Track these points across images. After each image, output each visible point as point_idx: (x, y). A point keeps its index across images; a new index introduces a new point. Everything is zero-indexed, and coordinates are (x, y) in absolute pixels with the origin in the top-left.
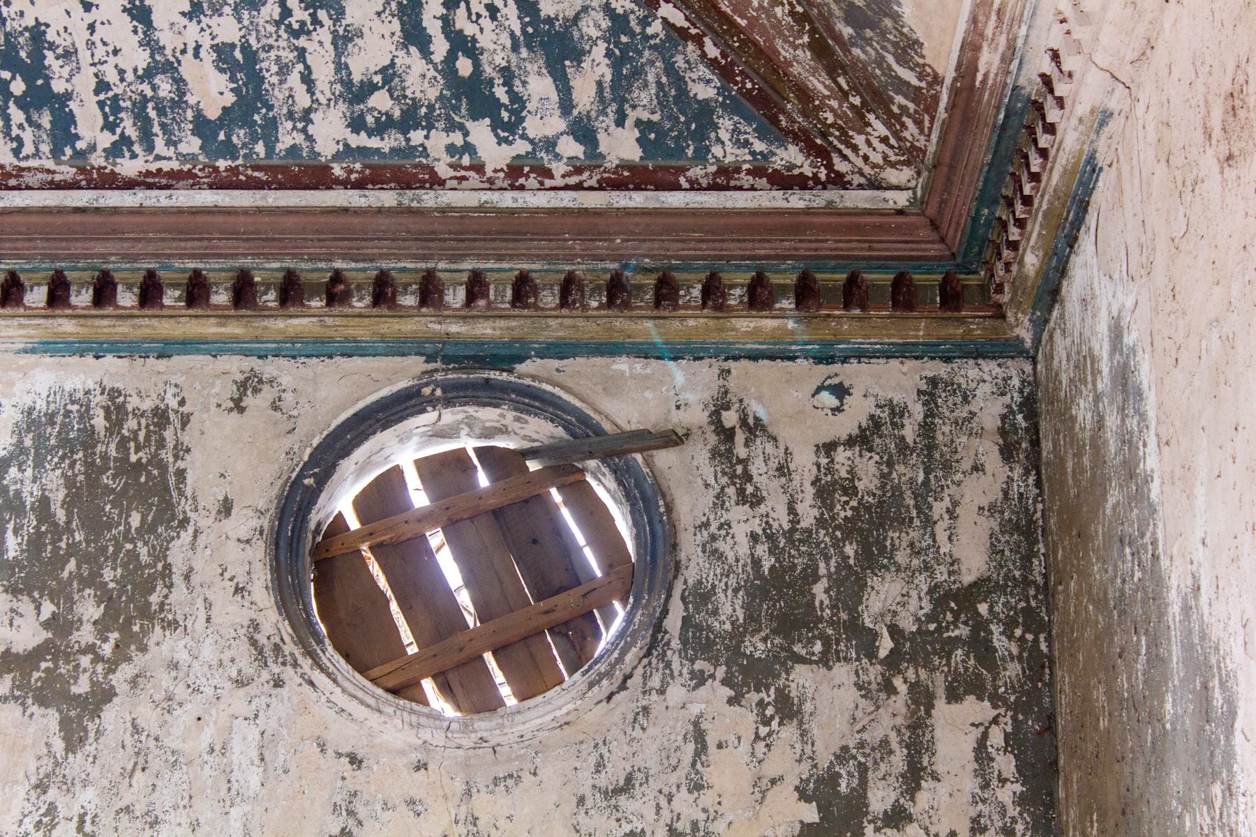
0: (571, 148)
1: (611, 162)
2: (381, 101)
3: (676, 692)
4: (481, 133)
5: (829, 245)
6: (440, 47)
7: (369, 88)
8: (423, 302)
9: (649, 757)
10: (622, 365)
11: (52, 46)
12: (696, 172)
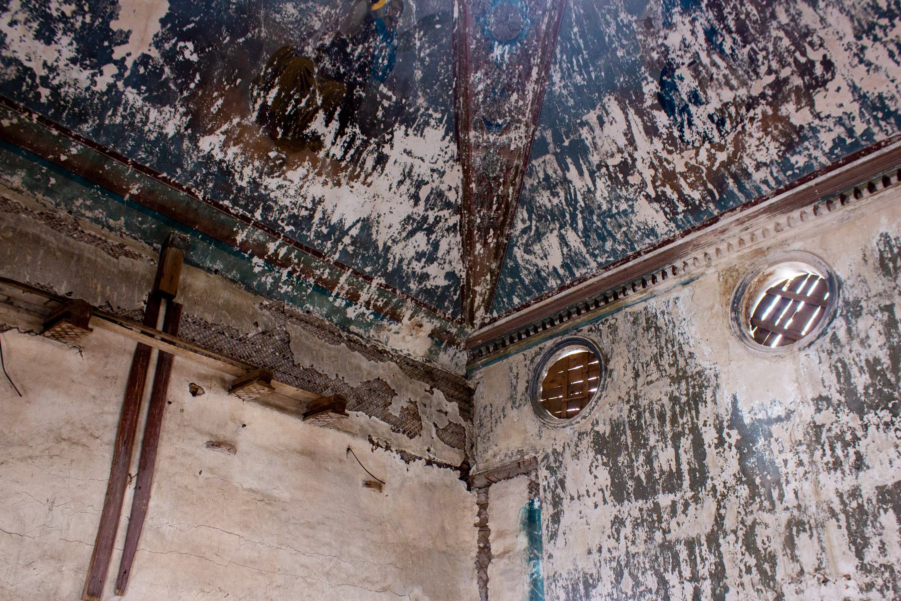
5: (552, 311)
11: (886, 98)
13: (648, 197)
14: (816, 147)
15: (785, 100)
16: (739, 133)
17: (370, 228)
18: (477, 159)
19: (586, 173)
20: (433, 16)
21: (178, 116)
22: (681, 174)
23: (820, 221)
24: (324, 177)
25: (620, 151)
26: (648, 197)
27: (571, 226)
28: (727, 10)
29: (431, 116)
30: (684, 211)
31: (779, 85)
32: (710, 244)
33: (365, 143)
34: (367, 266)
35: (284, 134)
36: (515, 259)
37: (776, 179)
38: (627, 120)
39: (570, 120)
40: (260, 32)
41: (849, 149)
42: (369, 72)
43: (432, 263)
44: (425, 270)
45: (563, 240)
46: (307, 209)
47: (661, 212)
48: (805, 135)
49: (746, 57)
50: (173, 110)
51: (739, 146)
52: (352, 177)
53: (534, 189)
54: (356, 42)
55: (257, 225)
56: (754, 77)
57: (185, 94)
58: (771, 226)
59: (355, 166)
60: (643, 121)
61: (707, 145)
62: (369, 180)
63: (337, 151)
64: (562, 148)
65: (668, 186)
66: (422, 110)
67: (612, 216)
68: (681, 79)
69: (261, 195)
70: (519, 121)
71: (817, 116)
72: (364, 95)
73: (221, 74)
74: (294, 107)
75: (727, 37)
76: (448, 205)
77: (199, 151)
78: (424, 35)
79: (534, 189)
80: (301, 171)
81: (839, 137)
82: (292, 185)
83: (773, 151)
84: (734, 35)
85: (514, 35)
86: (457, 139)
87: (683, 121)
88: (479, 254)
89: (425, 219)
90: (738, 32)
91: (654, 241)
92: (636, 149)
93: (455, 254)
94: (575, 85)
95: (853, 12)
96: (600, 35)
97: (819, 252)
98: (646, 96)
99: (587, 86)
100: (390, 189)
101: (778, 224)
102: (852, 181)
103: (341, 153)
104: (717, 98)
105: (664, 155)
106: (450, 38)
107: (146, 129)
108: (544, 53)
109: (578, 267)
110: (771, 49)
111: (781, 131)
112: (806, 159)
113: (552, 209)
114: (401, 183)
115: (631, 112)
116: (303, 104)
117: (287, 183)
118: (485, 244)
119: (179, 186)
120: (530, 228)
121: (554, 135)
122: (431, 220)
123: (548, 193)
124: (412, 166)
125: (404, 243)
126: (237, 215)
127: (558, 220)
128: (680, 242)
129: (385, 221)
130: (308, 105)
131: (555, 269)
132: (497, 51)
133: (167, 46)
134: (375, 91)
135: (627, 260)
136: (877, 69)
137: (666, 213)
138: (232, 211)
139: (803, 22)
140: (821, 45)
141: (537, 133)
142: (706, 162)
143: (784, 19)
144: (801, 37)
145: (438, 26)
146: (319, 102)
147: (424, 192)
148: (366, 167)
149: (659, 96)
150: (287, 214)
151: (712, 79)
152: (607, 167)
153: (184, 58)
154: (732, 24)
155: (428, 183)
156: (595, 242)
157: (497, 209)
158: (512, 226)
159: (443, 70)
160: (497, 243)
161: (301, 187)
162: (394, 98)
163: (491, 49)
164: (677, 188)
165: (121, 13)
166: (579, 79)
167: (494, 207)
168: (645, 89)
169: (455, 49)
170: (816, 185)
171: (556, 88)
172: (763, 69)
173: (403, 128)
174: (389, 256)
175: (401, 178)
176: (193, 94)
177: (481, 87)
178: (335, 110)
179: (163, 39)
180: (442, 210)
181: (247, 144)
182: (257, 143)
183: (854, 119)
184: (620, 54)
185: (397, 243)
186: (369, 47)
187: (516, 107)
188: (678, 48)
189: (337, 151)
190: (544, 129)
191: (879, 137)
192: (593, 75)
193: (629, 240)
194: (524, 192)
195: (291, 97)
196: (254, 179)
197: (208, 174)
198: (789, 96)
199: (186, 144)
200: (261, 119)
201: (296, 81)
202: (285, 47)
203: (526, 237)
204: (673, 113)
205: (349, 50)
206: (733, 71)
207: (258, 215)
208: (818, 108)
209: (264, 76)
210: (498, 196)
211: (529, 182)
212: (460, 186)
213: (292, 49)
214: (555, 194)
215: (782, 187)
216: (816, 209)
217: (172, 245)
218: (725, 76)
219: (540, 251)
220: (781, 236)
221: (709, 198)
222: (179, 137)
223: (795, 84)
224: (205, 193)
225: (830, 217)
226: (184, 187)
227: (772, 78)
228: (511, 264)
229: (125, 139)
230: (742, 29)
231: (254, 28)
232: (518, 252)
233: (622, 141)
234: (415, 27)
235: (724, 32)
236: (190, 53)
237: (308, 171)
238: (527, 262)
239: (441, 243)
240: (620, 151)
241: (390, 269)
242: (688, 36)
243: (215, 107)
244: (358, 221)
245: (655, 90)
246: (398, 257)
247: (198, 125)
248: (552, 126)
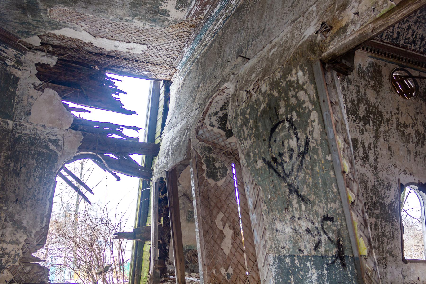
0: (418, 49)
2: (407, 41)
3: (420, 101)
4: (413, 46)
6: (414, 37)
7: (407, 39)
9: (418, 106)
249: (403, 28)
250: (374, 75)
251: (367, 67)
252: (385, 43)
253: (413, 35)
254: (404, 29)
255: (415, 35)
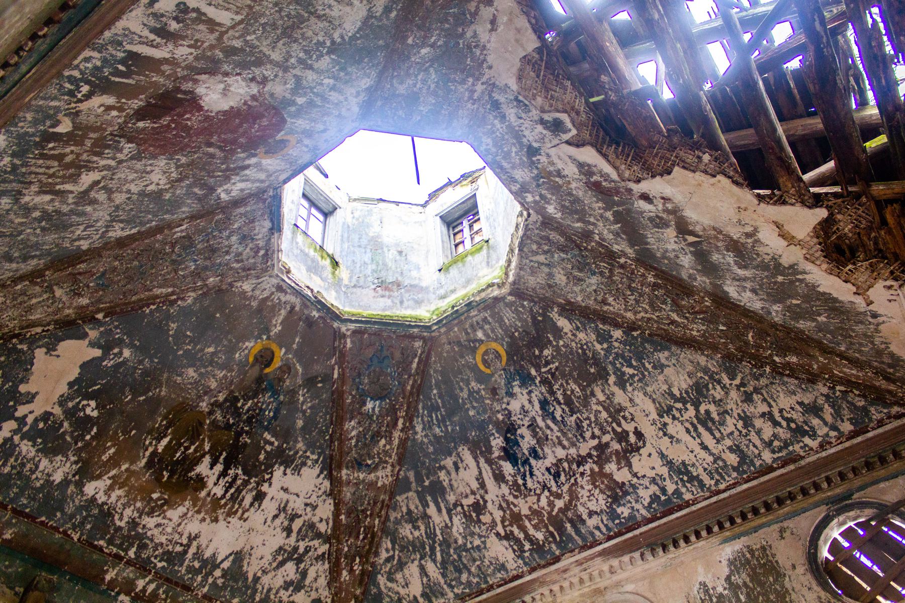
1: (847, 433)
2: (776, 443)
6: (784, 424)
8: (817, 490)
10: (882, 485)
12: (872, 425)
13: (498, 534)
14: (637, 501)
15: (608, 460)
16: (573, 484)
17: (242, 560)
18: (347, 493)
19: (444, 511)
20: (316, 377)
21: (68, 465)
22: (526, 516)
23: (647, 566)
24: (202, 514)
25: (473, 493)
26: (498, 534)
27: (430, 557)
28: (556, 387)
29: (308, 457)
30: (530, 549)
31: (602, 447)
32: (554, 582)
33: (246, 483)
34: (235, 597)
35: (169, 477)
36: (377, 586)
37: (606, 526)
38: (479, 468)
39: (430, 463)
40: (160, 391)
41: (665, 505)
42: (256, 422)
43: (299, 591)
44: (291, 599)
45: (423, 570)
46: (181, 545)
47: (510, 550)
48: (626, 490)
49: (573, 424)
50: (64, 459)
51: (574, 496)
52: (230, 514)
53: (397, 522)
54: (246, 398)
55: (129, 563)
56: (581, 440)
57: (80, 444)
58: (606, 568)
59: (234, 503)
60: (492, 469)
61: (546, 493)
62: (245, 516)
63: (219, 491)
64: (423, 487)
65: (515, 526)
66: (301, 453)
67: (467, 550)
68: (522, 437)
69: (138, 534)
70: (386, 462)
71: (635, 475)
72: (249, 441)
73: (117, 428)
74: (183, 453)
75: (557, 407)
76: (318, 535)
77: (82, 496)
78: (307, 392)
79: (397, 522)
80: (181, 510)
81: (655, 494)
82: (170, 523)
83: (602, 502)
84: (563, 406)
85: (385, 392)
86: (330, 477)
87: (525, 471)
88: (345, 580)
89: (296, 549)
90: (565, 404)
91: (505, 576)
92: (486, 492)
93: (323, 581)
94: (435, 436)
95: (654, 397)
96: (455, 398)
97: (649, 595)
98: (494, 449)
99: (445, 437)
100: (265, 523)
101: (612, 567)
102: (670, 532)
103: (222, 492)
104: (552, 454)
105: (511, 498)
106: (329, 393)
107: (34, 476)
108: (408, 407)
109: (437, 597)
110: (593, 419)
111: (606, 485)
112: (630, 511)
113: (413, 541)
114: (276, 517)
115: (482, 461)
116: (191, 451)
117: (166, 521)
118: (351, 571)
119: (56, 529)
120: (393, 557)
121: (415, 476)
122: (301, 550)
123: (410, 526)
124: (288, 501)
125: (273, 573)
126: (110, 555)
127: (419, 551)
128: (528, 578)
129: (257, 553)
130: (196, 451)
131: (415, 597)
132: (369, 405)
133: (70, 405)
134: (259, 438)
135: (481, 593)
136: (678, 441)
137: (514, 551)
138: (106, 551)
139: (617, 400)
140: (632, 419)
141: (401, 473)
142: (546, 508)
143: (602, 398)
144: (616, 412)
145: (320, 385)
146: (207, 448)
147: (297, 524)
148: (244, 504)
149: (504, 449)
150: (161, 551)
151: (547, 439)
152: (462, 506)
153: (85, 413)
154: (561, 398)
155: (301, 516)
156: (452, 574)
157: (364, 538)
158: (377, 554)
159: (322, 420)
160: (362, 570)
161: (180, 524)
162: (276, 444)
163: (364, 404)
164: (523, 529)
165: (32, 378)
166: (437, 430)
167: (361, 537)
168: (493, 443)
169: (333, 403)
170: (641, 534)
171: (418, 436)
172: (588, 435)
173: (282, 468)
174: (259, 587)
175: (276, 512)
176: (88, 444)
177: (354, 433)
178: (221, 454)
179: (68, 398)
180: (312, 540)
181: (132, 487)
182: (141, 486)
183: (665, 479)
184: (471, 413)
185: (267, 573)
186: (258, 402)
187: (384, 451)
188: (518, 412)
189: (219, 491)
190: (408, 470)
191: (687, 496)
192: (449, 428)
193: (483, 573)
194: (388, 524)
195: (182, 444)
196: (133, 519)
197: (89, 515)
198: (611, 457)
199: (72, 488)
200: (149, 464)
201: (188, 430)
202: (183, 403)
203: (389, 565)
204: (517, 464)
205: (239, 405)
206: (564, 434)
207: (131, 554)
208: (635, 469)
209: (158, 428)
210: (365, 527)
211: (393, 515)
212: (331, 517)
213: (188, 405)
214: (416, 528)
215: (612, 533)
216: (642, 555)
217: (36, 588)
218: (558, 437)
219: (402, 580)
220: (615, 578)
221: (551, 539)
222: (66, 482)
223: (615, 448)
224: (82, 535)
225: (656, 562)
226: (61, 530)
227: (595, 442)
228: (374, 590)
229: (10, 487)
230: (568, 402)
231: (155, 389)
232: (382, 580)
233: (475, 485)
234: (300, 386)
235: (555, 403)
236: (91, 410)
237: (188, 509)
238: (390, 589)
239: (309, 572)
240: (473, 493)
241: (257, 599)
242: (526, 404)
243: (107, 455)
244: (230, 555)
245: (501, 444)
246: (266, 587)
247: (86, 472)
248: (415, 468)
249: (732, 433)
250: (753, 590)
251: (728, 579)
252: (724, 491)
253: (776, 424)
254: (736, 433)
255: (779, 419)
